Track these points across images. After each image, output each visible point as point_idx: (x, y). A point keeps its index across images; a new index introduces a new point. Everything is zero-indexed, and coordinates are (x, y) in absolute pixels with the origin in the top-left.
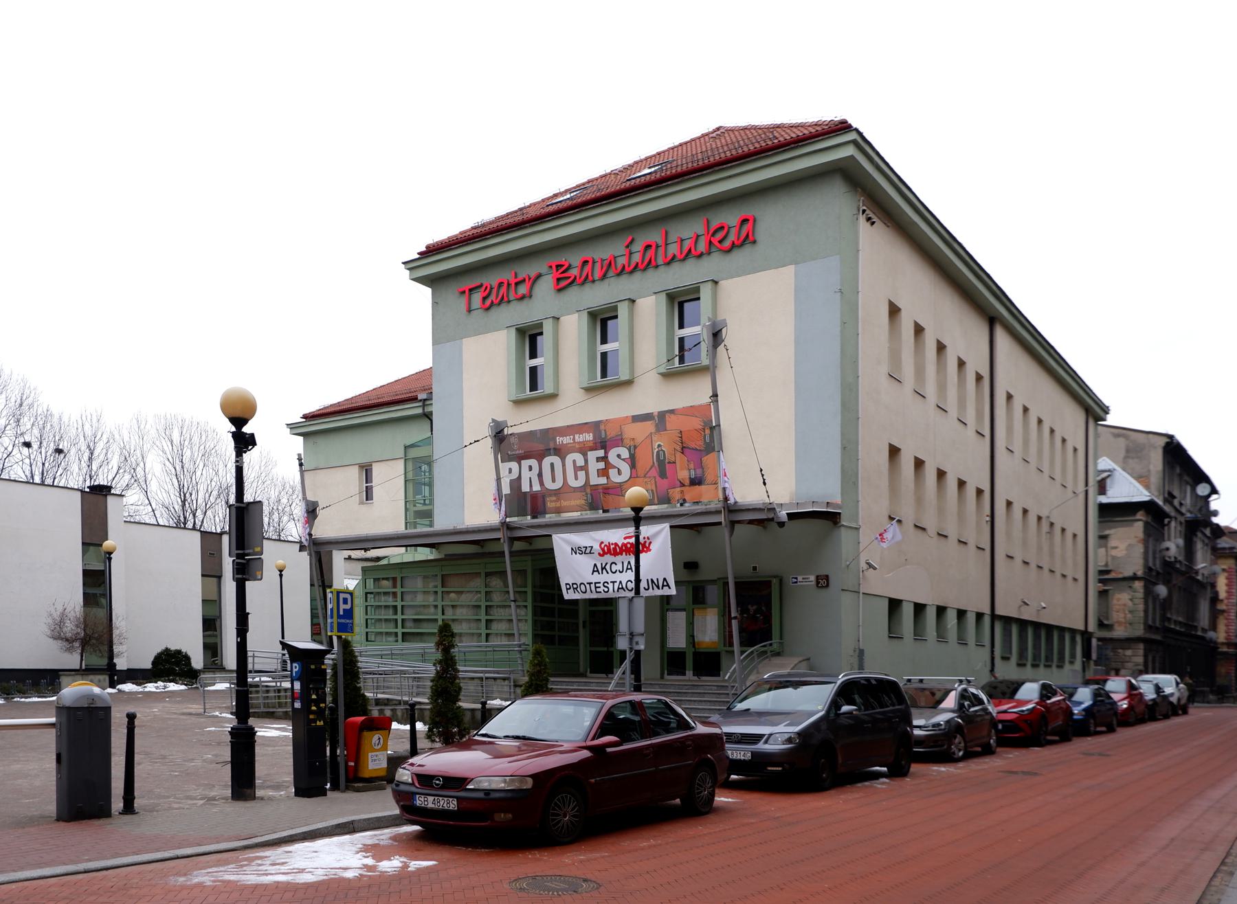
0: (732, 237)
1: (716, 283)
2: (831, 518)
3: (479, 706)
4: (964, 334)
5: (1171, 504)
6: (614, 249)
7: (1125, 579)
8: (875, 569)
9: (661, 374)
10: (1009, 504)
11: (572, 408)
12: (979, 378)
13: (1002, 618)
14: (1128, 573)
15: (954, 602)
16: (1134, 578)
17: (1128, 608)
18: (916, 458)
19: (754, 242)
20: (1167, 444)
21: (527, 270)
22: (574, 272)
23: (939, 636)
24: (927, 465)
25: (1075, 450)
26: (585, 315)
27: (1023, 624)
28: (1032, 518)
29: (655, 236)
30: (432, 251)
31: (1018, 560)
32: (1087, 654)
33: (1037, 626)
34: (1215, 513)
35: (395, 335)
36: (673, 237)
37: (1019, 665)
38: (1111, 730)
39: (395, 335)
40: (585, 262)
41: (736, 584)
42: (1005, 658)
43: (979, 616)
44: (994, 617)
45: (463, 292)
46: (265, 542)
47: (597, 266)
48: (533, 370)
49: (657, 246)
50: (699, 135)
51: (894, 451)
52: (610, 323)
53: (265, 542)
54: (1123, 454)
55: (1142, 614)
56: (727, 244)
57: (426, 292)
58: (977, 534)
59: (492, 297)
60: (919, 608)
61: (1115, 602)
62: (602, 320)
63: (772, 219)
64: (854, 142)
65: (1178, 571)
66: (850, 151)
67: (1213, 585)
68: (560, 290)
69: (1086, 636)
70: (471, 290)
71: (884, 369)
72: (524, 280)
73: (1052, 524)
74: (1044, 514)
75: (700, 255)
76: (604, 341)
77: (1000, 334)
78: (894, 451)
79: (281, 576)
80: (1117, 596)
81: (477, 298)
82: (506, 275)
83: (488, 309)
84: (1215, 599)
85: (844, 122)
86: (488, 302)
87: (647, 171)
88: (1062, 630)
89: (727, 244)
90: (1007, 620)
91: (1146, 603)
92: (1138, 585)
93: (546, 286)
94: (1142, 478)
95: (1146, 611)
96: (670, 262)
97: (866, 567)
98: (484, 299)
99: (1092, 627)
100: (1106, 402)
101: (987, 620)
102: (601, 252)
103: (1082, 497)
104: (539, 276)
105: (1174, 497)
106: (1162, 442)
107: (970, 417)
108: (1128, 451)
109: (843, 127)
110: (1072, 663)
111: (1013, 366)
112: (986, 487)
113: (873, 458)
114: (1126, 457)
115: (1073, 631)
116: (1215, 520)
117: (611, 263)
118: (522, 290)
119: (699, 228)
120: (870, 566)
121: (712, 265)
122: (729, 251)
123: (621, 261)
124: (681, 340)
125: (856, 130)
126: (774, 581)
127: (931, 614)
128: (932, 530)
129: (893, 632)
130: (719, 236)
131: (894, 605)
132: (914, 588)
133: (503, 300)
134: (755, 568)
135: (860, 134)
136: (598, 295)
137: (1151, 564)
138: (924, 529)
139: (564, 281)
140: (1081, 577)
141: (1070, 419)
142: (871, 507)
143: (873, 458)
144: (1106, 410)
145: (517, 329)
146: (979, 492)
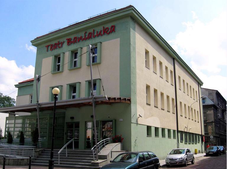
3: (29, 158)
4: (167, 63)
5: (219, 105)
7: (210, 122)
9: (87, 66)
12: (171, 72)
15: (167, 127)
16: (212, 122)
18: (180, 102)
20: (216, 92)
22: (72, 41)
24: (182, 103)
27: (186, 133)
32: (202, 141)
37: (185, 144)
38: (220, 155)
43: (174, 131)
44: (178, 131)
46: (132, 124)
51: (148, 87)
53: (132, 124)
54: (208, 94)
55: (214, 131)
56: (108, 32)
60: (157, 129)
61: (209, 128)
62: (75, 54)
65: (221, 121)
75: (102, 35)
77: (176, 62)
78: (148, 87)
80: (209, 127)
81: (50, 47)
85: (130, 6)
88: (196, 134)
89: (108, 32)
90: (182, 132)
91: (215, 128)
92: (214, 123)
93: (65, 44)
94: (212, 100)
95: (215, 130)
96: (94, 37)
97: (139, 116)
99: (203, 134)
100: (128, 5)
101: (176, 131)
104: (64, 42)
105: (219, 104)
106: (215, 92)
108: (209, 94)
110: (199, 143)
111: (179, 71)
114: (209, 95)
117: (81, 37)
118: (60, 45)
120: (140, 116)
121: (105, 37)
122: (109, 34)
131: (149, 128)
132: (155, 122)
136: (73, 47)
137: (216, 119)
141: (195, 85)
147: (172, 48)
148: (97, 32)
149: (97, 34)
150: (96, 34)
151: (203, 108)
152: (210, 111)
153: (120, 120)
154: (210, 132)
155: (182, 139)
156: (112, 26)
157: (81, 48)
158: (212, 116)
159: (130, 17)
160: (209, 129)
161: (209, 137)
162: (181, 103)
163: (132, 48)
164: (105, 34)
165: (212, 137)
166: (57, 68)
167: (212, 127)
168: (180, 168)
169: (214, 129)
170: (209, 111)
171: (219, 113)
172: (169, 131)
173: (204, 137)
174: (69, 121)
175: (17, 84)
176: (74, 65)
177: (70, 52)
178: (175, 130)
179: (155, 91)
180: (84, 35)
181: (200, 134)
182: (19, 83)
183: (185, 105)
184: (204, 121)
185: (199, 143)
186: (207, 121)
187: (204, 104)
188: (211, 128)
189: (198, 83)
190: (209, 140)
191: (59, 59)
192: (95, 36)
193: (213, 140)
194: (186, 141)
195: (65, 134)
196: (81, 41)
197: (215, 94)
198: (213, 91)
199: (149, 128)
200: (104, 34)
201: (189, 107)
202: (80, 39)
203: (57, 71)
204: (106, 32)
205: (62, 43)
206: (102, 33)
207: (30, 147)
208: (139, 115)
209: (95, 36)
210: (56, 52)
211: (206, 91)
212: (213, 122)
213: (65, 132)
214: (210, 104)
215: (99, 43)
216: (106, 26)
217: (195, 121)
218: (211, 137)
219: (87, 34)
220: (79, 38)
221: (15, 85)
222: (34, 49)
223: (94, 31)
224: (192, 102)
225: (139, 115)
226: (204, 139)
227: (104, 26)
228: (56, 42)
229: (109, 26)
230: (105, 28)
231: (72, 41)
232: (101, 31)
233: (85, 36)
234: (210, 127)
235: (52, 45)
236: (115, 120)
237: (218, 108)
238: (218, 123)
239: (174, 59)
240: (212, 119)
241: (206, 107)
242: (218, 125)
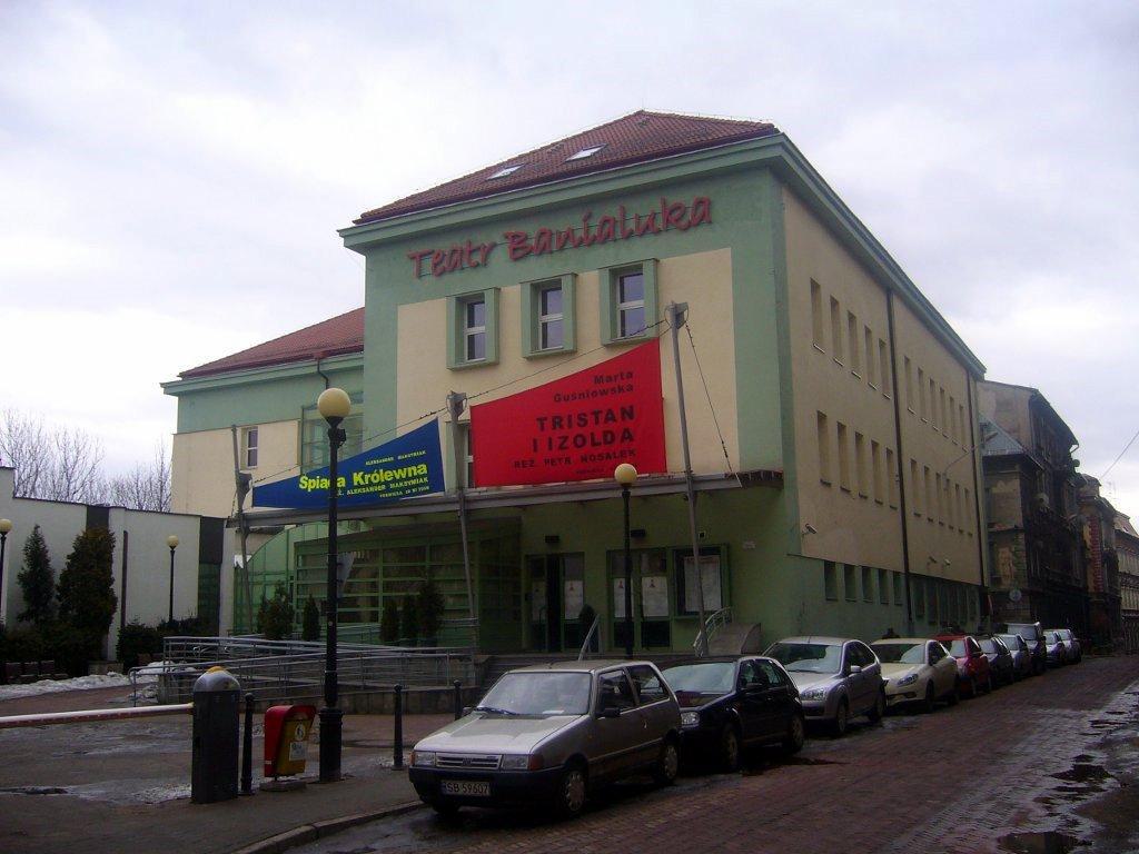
0: (689, 217)
1: (576, 275)
2: (779, 476)
6: (574, 222)
8: (815, 532)
10: (913, 462)
12: (882, 344)
13: (916, 576)
16: (1016, 530)
17: (1010, 560)
19: (710, 222)
21: (481, 239)
23: (866, 597)
25: (961, 408)
26: (607, 273)
28: (933, 477)
29: (612, 211)
30: (368, 219)
31: (924, 517)
34: (1077, 463)
36: (630, 215)
40: (543, 233)
42: (920, 617)
43: (896, 574)
45: (413, 258)
47: (555, 238)
49: (615, 222)
50: (580, 132)
51: (821, 418)
56: (684, 222)
57: (362, 259)
58: (890, 495)
59: (444, 264)
60: (849, 569)
61: (1000, 555)
62: (543, 291)
63: (724, 199)
64: (782, 144)
66: (778, 152)
67: (1081, 535)
68: (516, 259)
70: (421, 256)
72: (479, 249)
73: (948, 480)
74: (941, 471)
75: (658, 232)
76: (471, 325)
77: (897, 305)
78: (821, 418)
79: (173, 552)
80: (1001, 550)
81: (428, 263)
82: (459, 242)
83: (440, 275)
84: (1084, 547)
86: (440, 267)
87: (587, 153)
89: (684, 222)
92: (1021, 537)
93: (501, 256)
95: (1029, 565)
96: (628, 236)
97: (805, 531)
98: (435, 265)
101: (902, 577)
102: (559, 225)
104: (494, 245)
105: (1043, 449)
106: (1027, 396)
108: (998, 402)
109: (769, 130)
112: (894, 448)
113: (805, 425)
116: (1078, 470)
117: (569, 235)
118: (477, 258)
119: (658, 208)
120: (933, 560)
121: (674, 238)
122: (685, 229)
123: (580, 234)
124: (623, 312)
125: (783, 134)
127: (858, 574)
128: (855, 493)
130: (676, 214)
131: (829, 566)
133: (454, 268)
136: (540, 268)
138: (849, 491)
139: (520, 250)
140: (974, 531)
142: (805, 473)
143: (805, 425)
145: (532, 285)
146: (889, 452)
147: (803, 158)
149: (638, 223)
150: (631, 225)
153: (744, 547)
154: (1008, 573)
156: (700, 202)
157: (572, 274)
158: (1017, 503)
164: (671, 227)
165: (1015, 594)
167: (1014, 553)
168: (553, 836)
170: (1001, 483)
172: (882, 573)
174: (542, 549)
175: (174, 377)
177: (528, 286)
179: (841, 428)
182: (181, 375)
184: (991, 525)
188: (1011, 555)
189: (964, 371)
192: (632, 232)
195: (523, 598)
202: (567, 240)
203: (467, 362)
205: (489, 250)
206: (659, 223)
207: (423, 652)
210: (466, 282)
212: (1021, 531)
213: (523, 591)
214: (1007, 452)
215: (651, 264)
216: (673, 199)
217: (845, 491)
218: (1012, 596)
221: (162, 385)
222: (359, 261)
231: (532, 242)
232: (653, 216)
233: (587, 229)
234: (1006, 550)
235: (439, 259)
236: (728, 547)
240: (1014, 516)
242: (1041, 543)
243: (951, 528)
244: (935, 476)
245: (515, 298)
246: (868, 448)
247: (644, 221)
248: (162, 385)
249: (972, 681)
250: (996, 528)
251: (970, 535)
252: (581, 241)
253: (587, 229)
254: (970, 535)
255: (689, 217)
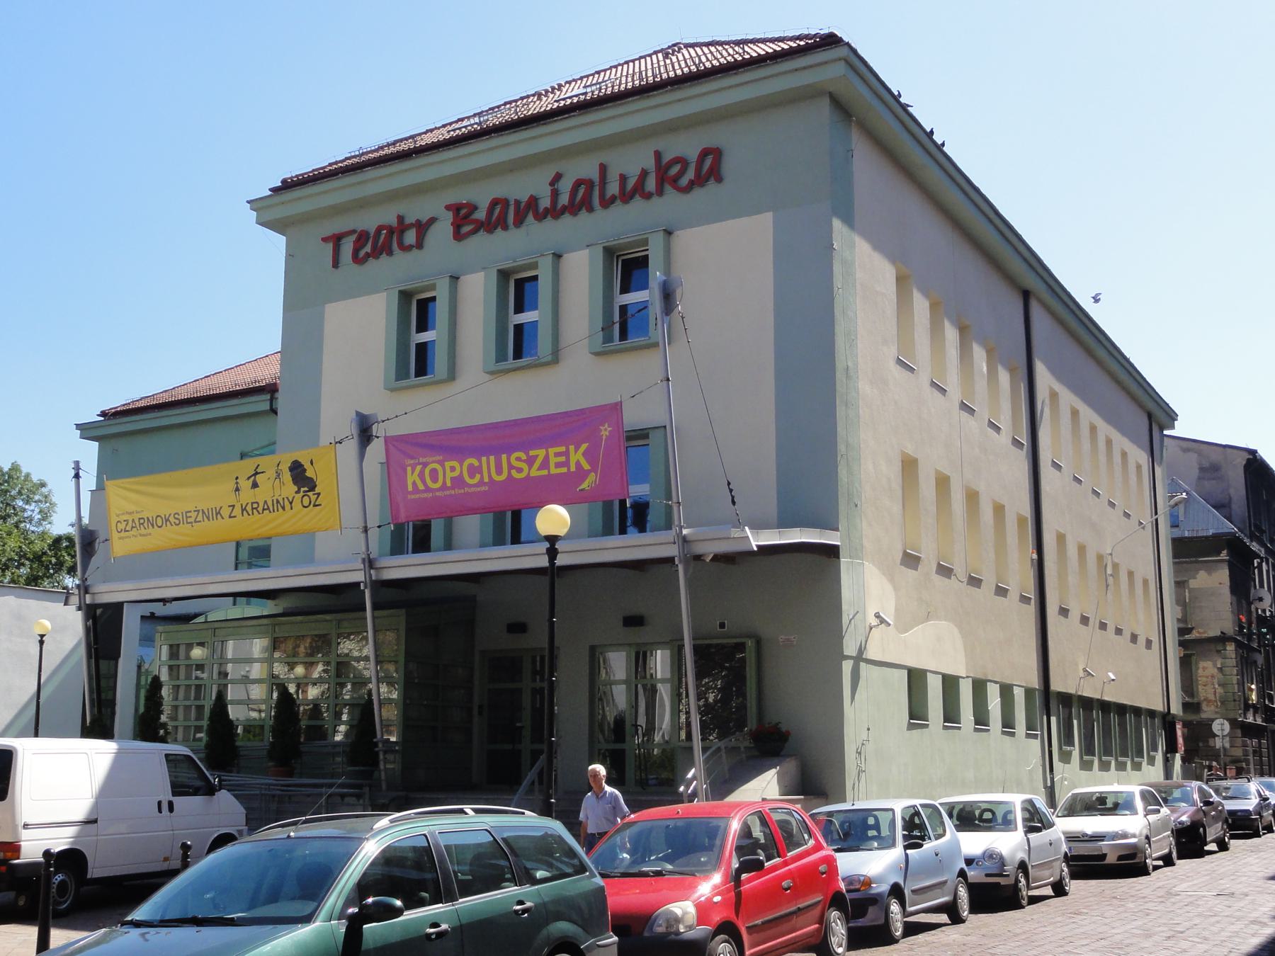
11: (477, 393)
14: (1214, 632)
16: (1223, 639)
30: (288, 185)
31: (1111, 628)
32: (1171, 748)
33: (1105, 706)
35: (224, 312)
39: (224, 312)
41: (697, 650)
48: (422, 349)
51: (909, 466)
52: (527, 286)
54: (1195, 473)
56: (684, 181)
58: (1020, 578)
59: (368, 248)
61: (1200, 671)
62: (518, 288)
69: (1168, 722)
71: (892, 351)
77: (1036, 311)
79: (41, 642)
80: (1202, 664)
81: (347, 247)
88: (1137, 711)
89: (684, 181)
90: (1066, 700)
92: (1231, 647)
94: (1222, 506)
96: (607, 203)
97: (874, 622)
99: (1176, 709)
103: (1149, 528)
104: (432, 220)
105: (1262, 532)
106: (1241, 460)
107: (1005, 422)
108: (1202, 469)
109: (831, 41)
110: (1152, 761)
114: (1199, 478)
115: (1152, 713)
117: (533, 201)
118: (410, 237)
120: (882, 621)
121: (671, 204)
125: (848, 44)
126: (750, 643)
129: (917, 714)
131: (916, 678)
134: (722, 625)
135: (854, 51)
144: (1171, 417)
148: (623, 179)
150: (613, 188)
151: (1175, 556)
152: (1209, 572)
154: (1211, 697)
155: (1067, 738)
159: (826, 98)
160: (1202, 680)
161: (1207, 725)
162: (1061, 538)
163: (837, 268)
165: (1221, 727)
166: (416, 363)
167: (1220, 670)
169: (1235, 679)
170: (1202, 575)
171: (1262, 586)
173: (1179, 726)
176: (517, 346)
178: (1034, 689)
179: (943, 482)
180: (549, 188)
181: (1159, 706)
182: (103, 414)
183: (1082, 549)
184: (1182, 632)
185: (1152, 761)
186: (1189, 631)
187: (1177, 533)
190: (1211, 743)
191: (425, 307)
192: (613, 199)
193: (1227, 745)
194: (1088, 749)
196: (530, 218)
197: (1241, 471)
198: (1229, 450)
199: (916, 678)
200: (660, 192)
201: (1100, 558)
204: (674, 181)
205: (422, 228)
206: (651, 184)
208: (877, 616)
209: (613, 199)
210: (399, 268)
211: (1186, 450)
214: (1211, 532)
218: (1216, 727)
219: (565, 186)
220: (517, 202)
221: (78, 426)
223: (603, 169)
224: (1113, 521)
225: (877, 616)
226: (1180, 740)
227: (659, 144)
228: (388, 216)
229: (687, 146)
230: (667, 158)
232: (644, 174)
233: (555, 194)
234: (1208, 664)
235: (362, 237)
236: (759, 642)
237: (1258, 556)
238: (1255, 645)
239: (1026, 295)
240: (1219, 615)
241: (1189, 550)
243: (1103, 626)
244: (892, 472)
245: (478, 292)
246: (927, 488)
247: (631, 183)
248: (78, 426)
249: (895, 907)
250: (1194, 635)
251: (1064, 612)
252: (547, 211)
253: (555, 194)
254: (1064, 612)
255: (690, 174)
